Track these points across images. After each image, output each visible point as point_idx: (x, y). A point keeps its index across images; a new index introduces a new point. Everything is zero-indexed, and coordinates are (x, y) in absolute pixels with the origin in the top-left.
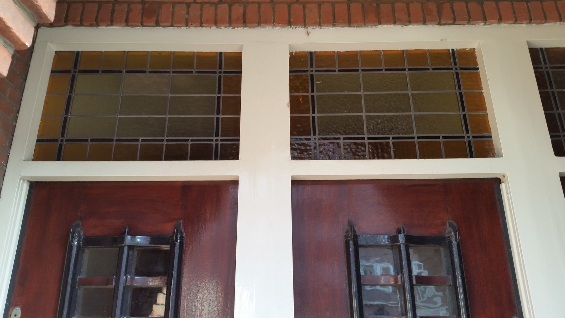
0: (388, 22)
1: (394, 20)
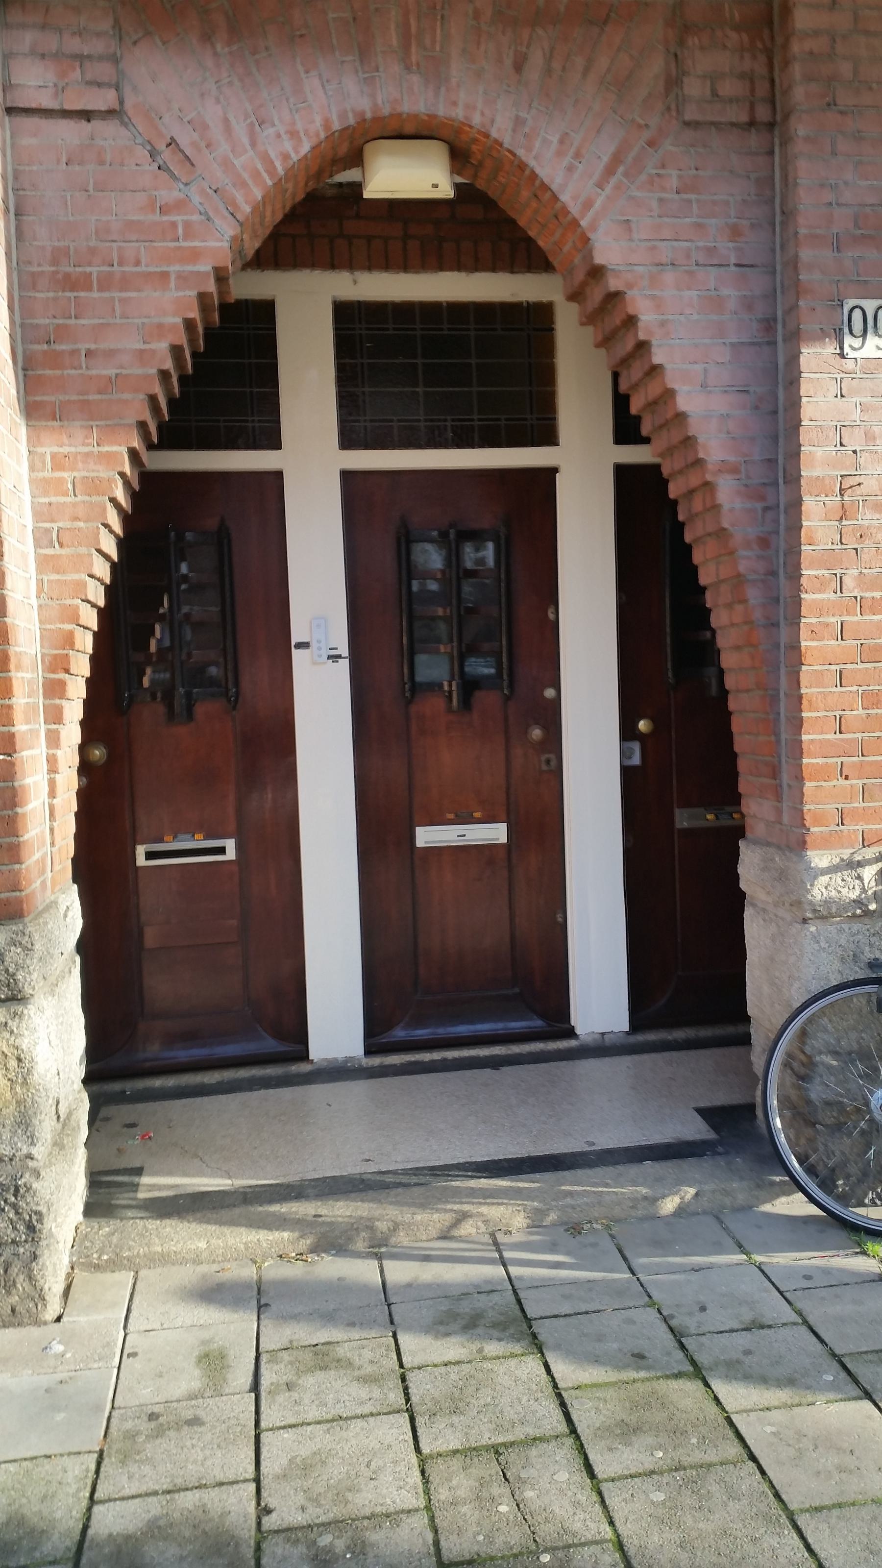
0: (451, 269)
1: (459, 266)
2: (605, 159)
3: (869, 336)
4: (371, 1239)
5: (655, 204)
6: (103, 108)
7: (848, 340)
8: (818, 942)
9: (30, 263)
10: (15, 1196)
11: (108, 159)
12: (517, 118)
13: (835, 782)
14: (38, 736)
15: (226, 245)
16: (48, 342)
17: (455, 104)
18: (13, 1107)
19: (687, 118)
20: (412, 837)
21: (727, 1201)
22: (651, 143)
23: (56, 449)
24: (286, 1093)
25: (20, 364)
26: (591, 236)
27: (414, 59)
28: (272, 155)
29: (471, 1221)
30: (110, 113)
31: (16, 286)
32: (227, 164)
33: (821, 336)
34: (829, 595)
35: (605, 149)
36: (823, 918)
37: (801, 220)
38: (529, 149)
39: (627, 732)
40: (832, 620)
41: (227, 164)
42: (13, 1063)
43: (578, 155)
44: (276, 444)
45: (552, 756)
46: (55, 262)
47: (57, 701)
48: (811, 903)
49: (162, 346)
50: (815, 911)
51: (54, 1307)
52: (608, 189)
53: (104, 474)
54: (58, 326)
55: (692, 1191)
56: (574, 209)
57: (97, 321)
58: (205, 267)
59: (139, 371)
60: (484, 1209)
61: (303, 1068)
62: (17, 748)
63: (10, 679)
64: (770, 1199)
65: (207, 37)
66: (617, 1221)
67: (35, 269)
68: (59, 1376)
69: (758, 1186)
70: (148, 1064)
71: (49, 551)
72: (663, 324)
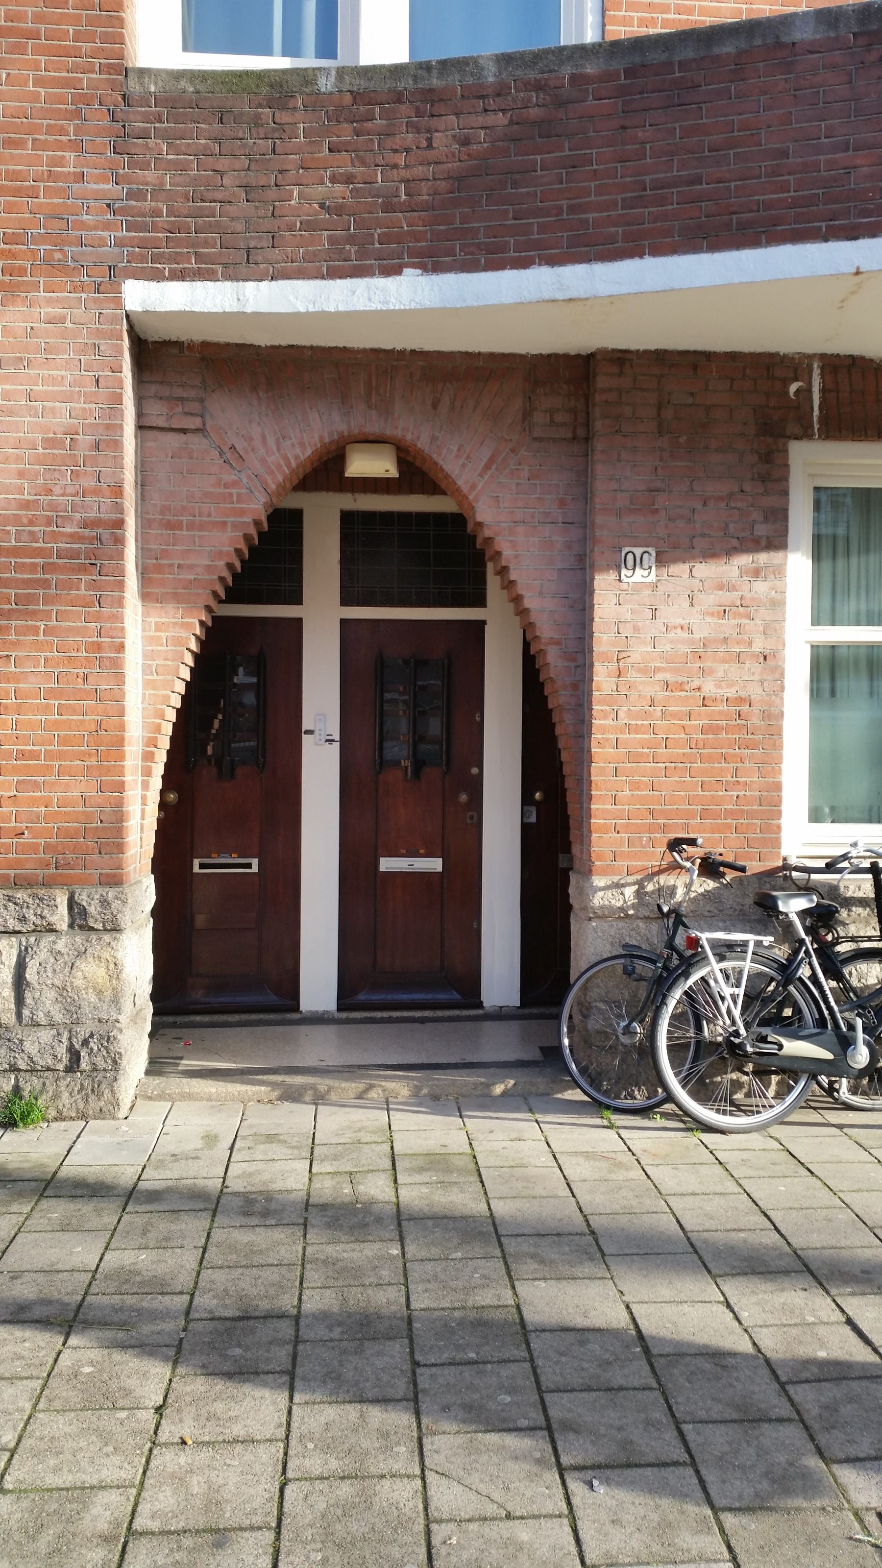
2: (485, 460)
3: (637, 569)
4: (315, 1095)
5: (513, 487)
6: (194, 428)
7: (624, 572)
8: (596, 932)
9: (148, 513)
10: (108, 1042)
11: (195, 455)
12: (433, 435)
13: (611, 835)
14: (137, 784)
15: (261, 507)
16: (157, 559)
17: (396, 427)
18: (110, 992)
19: (536, 435)
20: (377, 864)
21: (533, 1089)
22: (512, 451)
23: (157, 620)
24: (280, 1029)
25: (140, 571)
26: (474, 504)
27: (373, 401)
28: (290, 456)
29: (374, 1090)
30: (197, 430)
31: (139, 526)
32: (263, 461)
33: (607, 568)
34: (609, 722)
35: (485, 454)
36: (599, 917)
37: (597, 500)
38: (440, 455)
39: (527, 799)
40: (611, 736)
41: (263, 461)
42: (112, 966)
43: (468, 458)
44: (300, 602)
45: (475, 814)
46: (162, 513)
47: (149, 764)
48: (592, 908)
49: (221, 563)
50: (594, 913)
51: (123, 1112)
52: (486, 477)
53: (184, 634)
54: (163, 550)
55: (512, 1082)
56: (465, 489)
57: (185, 548)
58: (248, 519)
59: (208, 577)
60: (383, 1084)
61: (295, 1016)
62: (126, 789)
63: (124, 751)
64: (562, 1091)
65: (254, 388)
66: (464, 1096)
67: (151, 517)
68: (125, 1139)
69: (553, 1081)
70: (192, 1007)
71: (151, 677)
72: (516, 557)
